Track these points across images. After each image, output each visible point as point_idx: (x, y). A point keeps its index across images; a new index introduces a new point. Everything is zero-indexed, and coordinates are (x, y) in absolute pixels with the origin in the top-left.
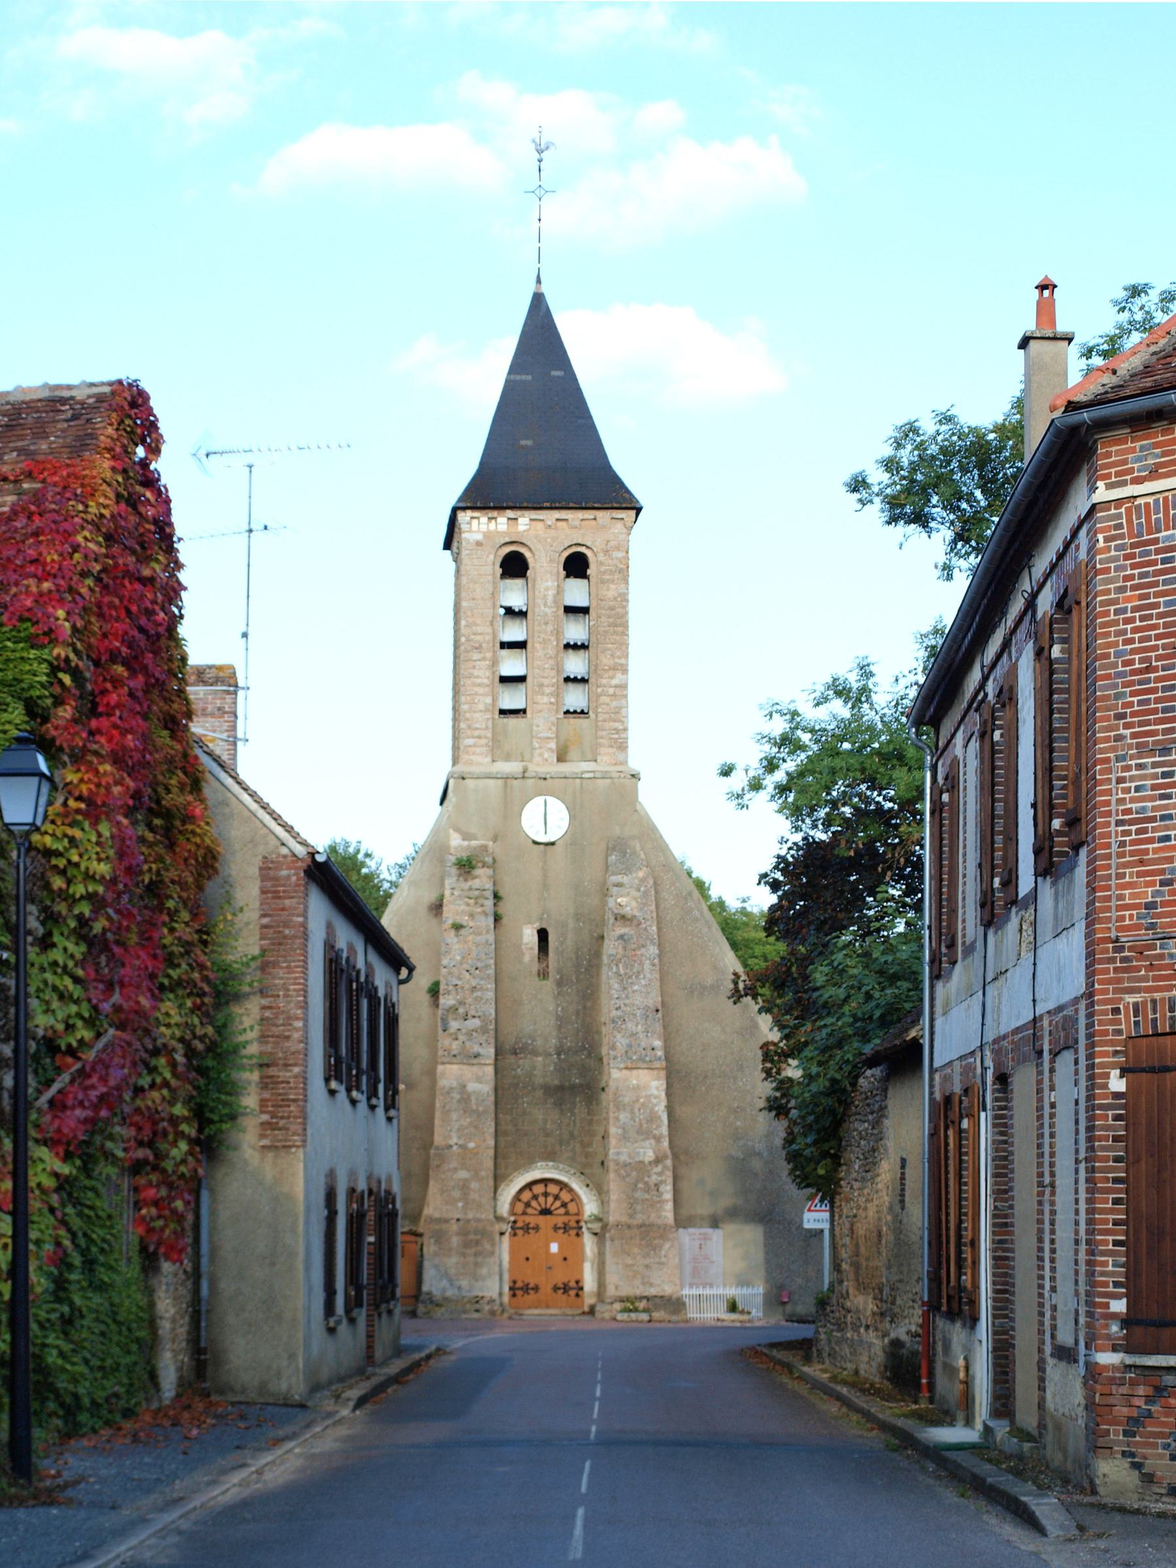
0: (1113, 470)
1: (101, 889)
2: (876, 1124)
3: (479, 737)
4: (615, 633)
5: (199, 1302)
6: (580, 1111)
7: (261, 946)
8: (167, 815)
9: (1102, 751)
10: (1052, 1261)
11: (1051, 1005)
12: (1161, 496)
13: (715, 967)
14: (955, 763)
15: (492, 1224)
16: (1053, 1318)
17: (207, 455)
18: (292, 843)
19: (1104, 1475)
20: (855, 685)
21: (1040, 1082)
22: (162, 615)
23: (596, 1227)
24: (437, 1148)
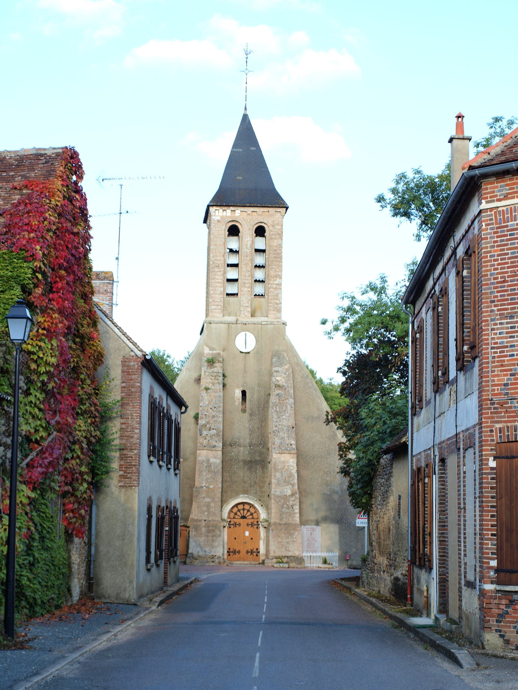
0: (489, 195)
1: (52, 369)
2: (388, 480)
3: (218, 305)
5: (90, 556)
6: (259, 472)
7: (121, 396)
8: (82, 337)
9: (485, 317)
10: (465, 542)
11: (464, 428)
12: (509, 207)
13: (318, 409)
14: (422, 321)
15: (220, 523)
16: (465, 568)
17: (103, 180)
18: (136, 350)
19: (488, 640)
20: (379, 286)
21: (459, 462)
22: (82, 249)
23: (266, 524)
24: (197, 488)
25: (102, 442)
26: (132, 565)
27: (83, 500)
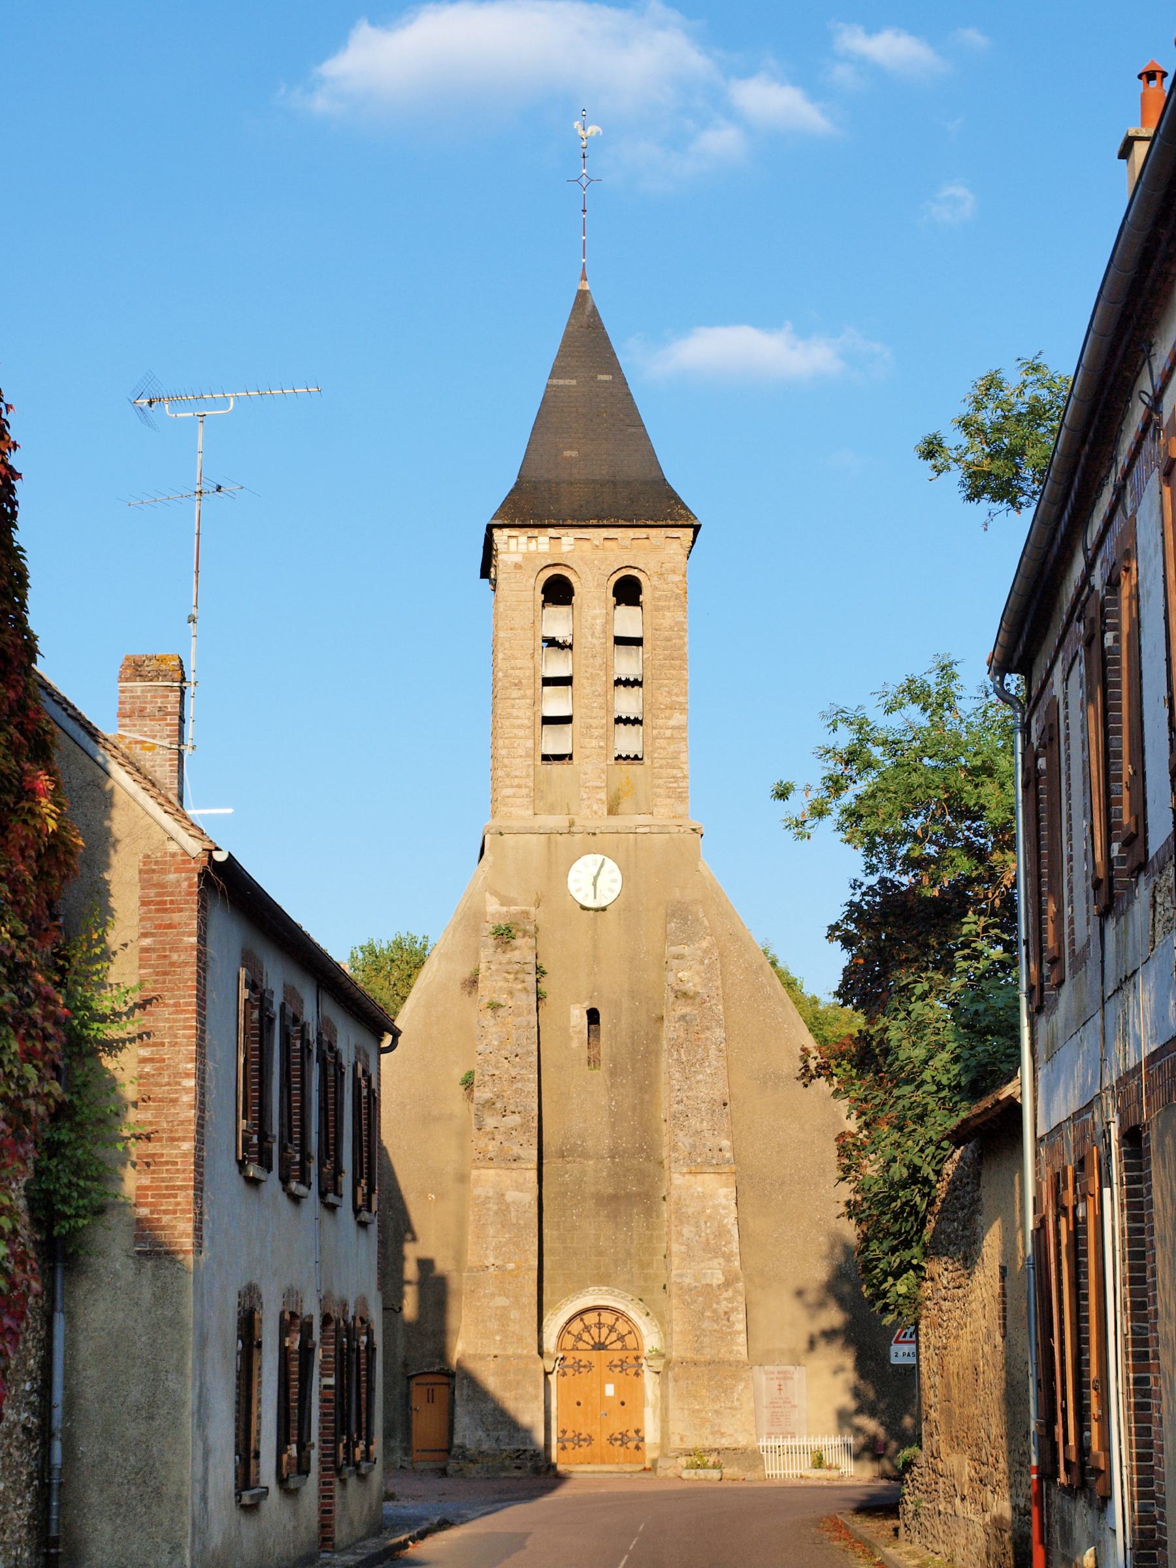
3: (519, 786)
4: (673, 667)
14: (1054, 705)
23: (659, 1364)
24: (471, 1270)
25: (78, 1118)
26: (179, 1496)
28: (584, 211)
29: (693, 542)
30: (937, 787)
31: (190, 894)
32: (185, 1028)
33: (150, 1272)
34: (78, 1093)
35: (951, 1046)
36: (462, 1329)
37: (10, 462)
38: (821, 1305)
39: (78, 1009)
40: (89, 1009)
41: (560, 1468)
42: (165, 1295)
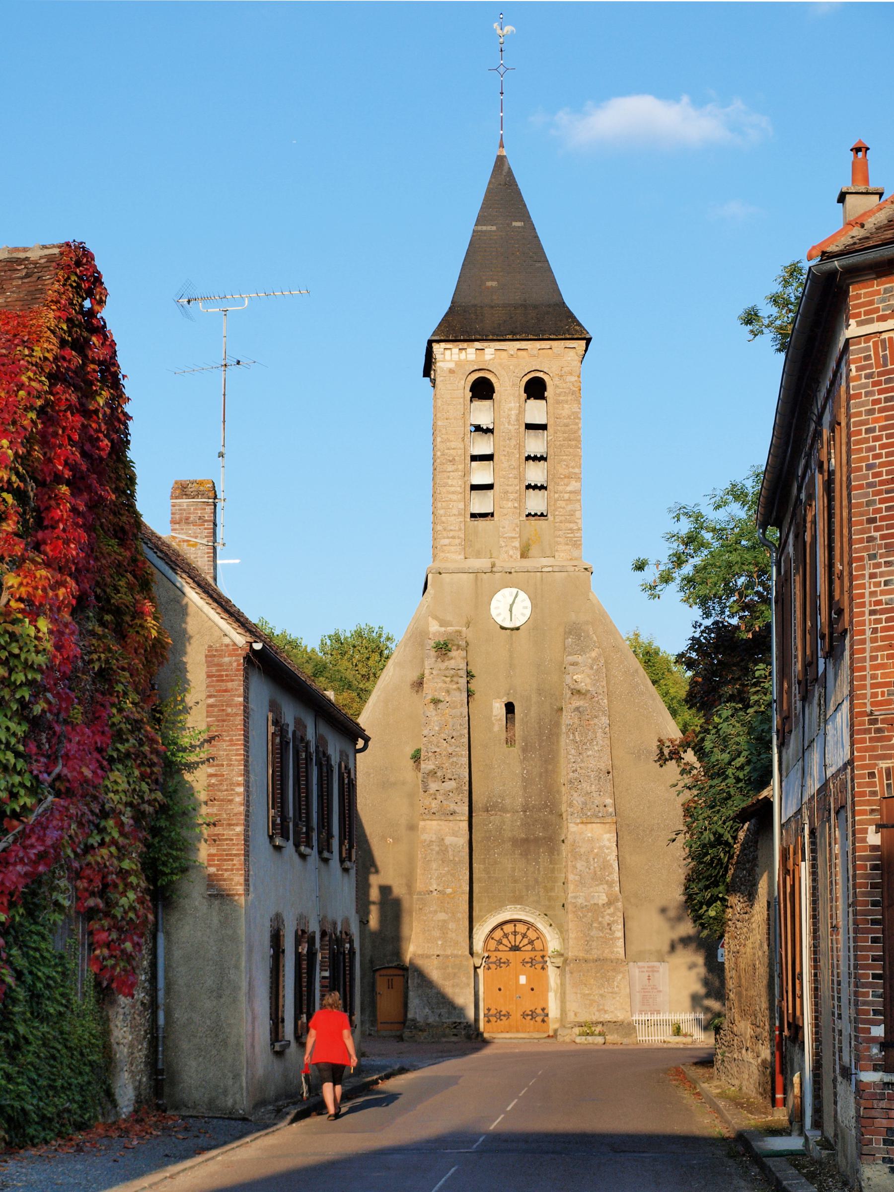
0: (862, 310)
1: (39, 677)
3: (453, 537)
4: (570, 446)
5: (157, 1029)
8: (118, 612)
19: (869, 1179)
22: (106, 442)
23: (559, 961)
24: (419, 893)
25: (171, 813)
26: (238, 1044)
27: (127, 924)
28: (502, 93)
29: (586, 351)
30: (750, 563)
31: (238, 670)
32: (237, 755)
33: (217, 908)
34: (170, 797)
35: (745, 753)
36: (413, 936)
37: (125, 410)
38: (679, 919)
39: (169, 744)
40: (176, 744)
41: (486, 1035)
42: (227, 921)
